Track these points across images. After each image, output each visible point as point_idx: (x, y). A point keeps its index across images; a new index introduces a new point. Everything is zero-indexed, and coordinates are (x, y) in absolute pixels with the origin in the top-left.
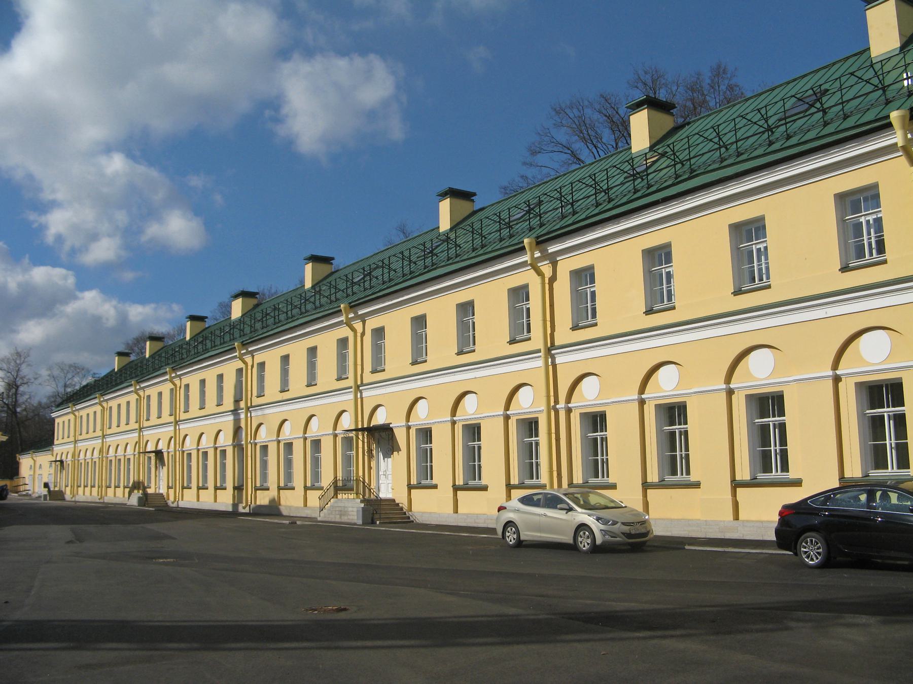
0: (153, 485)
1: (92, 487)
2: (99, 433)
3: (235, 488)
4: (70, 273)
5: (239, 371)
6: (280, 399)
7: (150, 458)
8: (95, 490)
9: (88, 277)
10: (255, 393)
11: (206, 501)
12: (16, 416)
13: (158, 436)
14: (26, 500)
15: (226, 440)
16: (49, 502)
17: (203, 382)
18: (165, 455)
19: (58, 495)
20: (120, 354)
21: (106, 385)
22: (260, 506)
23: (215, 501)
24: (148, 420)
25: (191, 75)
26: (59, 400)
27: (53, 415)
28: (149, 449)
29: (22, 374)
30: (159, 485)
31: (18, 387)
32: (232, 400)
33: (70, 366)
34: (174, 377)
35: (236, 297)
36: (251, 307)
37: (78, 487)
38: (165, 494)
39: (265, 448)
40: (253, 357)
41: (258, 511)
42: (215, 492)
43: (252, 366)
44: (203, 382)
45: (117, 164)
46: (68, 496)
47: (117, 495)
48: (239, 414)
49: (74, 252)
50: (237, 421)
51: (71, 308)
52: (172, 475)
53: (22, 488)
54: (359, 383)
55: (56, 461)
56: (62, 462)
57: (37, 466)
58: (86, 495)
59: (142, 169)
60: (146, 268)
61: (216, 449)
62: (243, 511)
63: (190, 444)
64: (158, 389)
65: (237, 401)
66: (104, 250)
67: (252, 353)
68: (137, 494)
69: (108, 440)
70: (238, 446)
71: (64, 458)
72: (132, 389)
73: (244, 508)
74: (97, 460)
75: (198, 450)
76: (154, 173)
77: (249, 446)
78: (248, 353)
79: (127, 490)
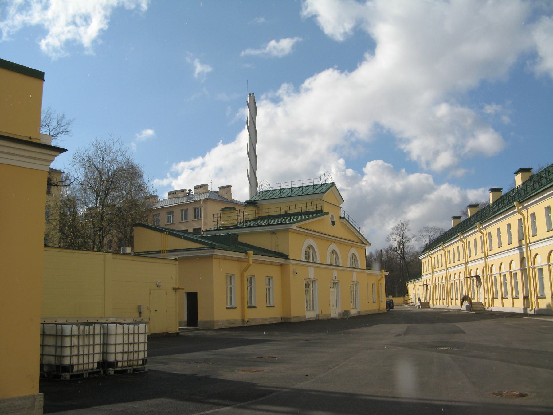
0: (476, 297)
2: (444, 267)
3: (524, 298)
4: (430, 175)
5: (520, 220)
7: (473, 281)
8: (445, 301)
9: (440, 177)
10: (531, 234)
11: (508, 306)
12: (405, 260)
13: (476, 267)
14: (411, 309)
15: (516, 266)
16: (421, 310)
17: (499, 230)
19: (426, 305)
20: (454, 218)
21: (446, 237)
22: (541, 309)
24: (470, 257)
25: (482, 49)
26: (422, 249)
28: (472, 275)
29: (405, 235)
31: (404, 243)
32: (517, 240)
33: (432, 229)
34: (482, 229)
35: (517, 173)
36: (528, 178)
37: (437, 300)
38: (483, 303)
39: (541, 270)
40: (527, 210)
41: (540, 313)
42: (513, 301)
43: (528, 217)
44: (499, 230)
45: (443, 110)
46: (431, 306)
47: (456, 305)
48: (522, 249)
49: (428, 163)
50: (521, 253)
51: (433, 196)
52: (486, 292)
53: (410, 301)
54: (528, 242)
55: (424, 285)
56: (427, 285)
57: (417, 288)
58: (440, 305)
59: (459, 109)
60: (472, 165)
61: (511, 272)
62: (531, 313)
63: (495, 271)
64: (474, 237)
65: (520, 241)
66: (444, 159)
67: (526, 208)
68: (466, 303)
69: (449, 271)
70: (523, 270)
71: (428, 283)
72: (459, 238)
73: (531, 311)
74: (445, 283)
76: (465, 110)
77: (531, 269)
78: (524, 208)
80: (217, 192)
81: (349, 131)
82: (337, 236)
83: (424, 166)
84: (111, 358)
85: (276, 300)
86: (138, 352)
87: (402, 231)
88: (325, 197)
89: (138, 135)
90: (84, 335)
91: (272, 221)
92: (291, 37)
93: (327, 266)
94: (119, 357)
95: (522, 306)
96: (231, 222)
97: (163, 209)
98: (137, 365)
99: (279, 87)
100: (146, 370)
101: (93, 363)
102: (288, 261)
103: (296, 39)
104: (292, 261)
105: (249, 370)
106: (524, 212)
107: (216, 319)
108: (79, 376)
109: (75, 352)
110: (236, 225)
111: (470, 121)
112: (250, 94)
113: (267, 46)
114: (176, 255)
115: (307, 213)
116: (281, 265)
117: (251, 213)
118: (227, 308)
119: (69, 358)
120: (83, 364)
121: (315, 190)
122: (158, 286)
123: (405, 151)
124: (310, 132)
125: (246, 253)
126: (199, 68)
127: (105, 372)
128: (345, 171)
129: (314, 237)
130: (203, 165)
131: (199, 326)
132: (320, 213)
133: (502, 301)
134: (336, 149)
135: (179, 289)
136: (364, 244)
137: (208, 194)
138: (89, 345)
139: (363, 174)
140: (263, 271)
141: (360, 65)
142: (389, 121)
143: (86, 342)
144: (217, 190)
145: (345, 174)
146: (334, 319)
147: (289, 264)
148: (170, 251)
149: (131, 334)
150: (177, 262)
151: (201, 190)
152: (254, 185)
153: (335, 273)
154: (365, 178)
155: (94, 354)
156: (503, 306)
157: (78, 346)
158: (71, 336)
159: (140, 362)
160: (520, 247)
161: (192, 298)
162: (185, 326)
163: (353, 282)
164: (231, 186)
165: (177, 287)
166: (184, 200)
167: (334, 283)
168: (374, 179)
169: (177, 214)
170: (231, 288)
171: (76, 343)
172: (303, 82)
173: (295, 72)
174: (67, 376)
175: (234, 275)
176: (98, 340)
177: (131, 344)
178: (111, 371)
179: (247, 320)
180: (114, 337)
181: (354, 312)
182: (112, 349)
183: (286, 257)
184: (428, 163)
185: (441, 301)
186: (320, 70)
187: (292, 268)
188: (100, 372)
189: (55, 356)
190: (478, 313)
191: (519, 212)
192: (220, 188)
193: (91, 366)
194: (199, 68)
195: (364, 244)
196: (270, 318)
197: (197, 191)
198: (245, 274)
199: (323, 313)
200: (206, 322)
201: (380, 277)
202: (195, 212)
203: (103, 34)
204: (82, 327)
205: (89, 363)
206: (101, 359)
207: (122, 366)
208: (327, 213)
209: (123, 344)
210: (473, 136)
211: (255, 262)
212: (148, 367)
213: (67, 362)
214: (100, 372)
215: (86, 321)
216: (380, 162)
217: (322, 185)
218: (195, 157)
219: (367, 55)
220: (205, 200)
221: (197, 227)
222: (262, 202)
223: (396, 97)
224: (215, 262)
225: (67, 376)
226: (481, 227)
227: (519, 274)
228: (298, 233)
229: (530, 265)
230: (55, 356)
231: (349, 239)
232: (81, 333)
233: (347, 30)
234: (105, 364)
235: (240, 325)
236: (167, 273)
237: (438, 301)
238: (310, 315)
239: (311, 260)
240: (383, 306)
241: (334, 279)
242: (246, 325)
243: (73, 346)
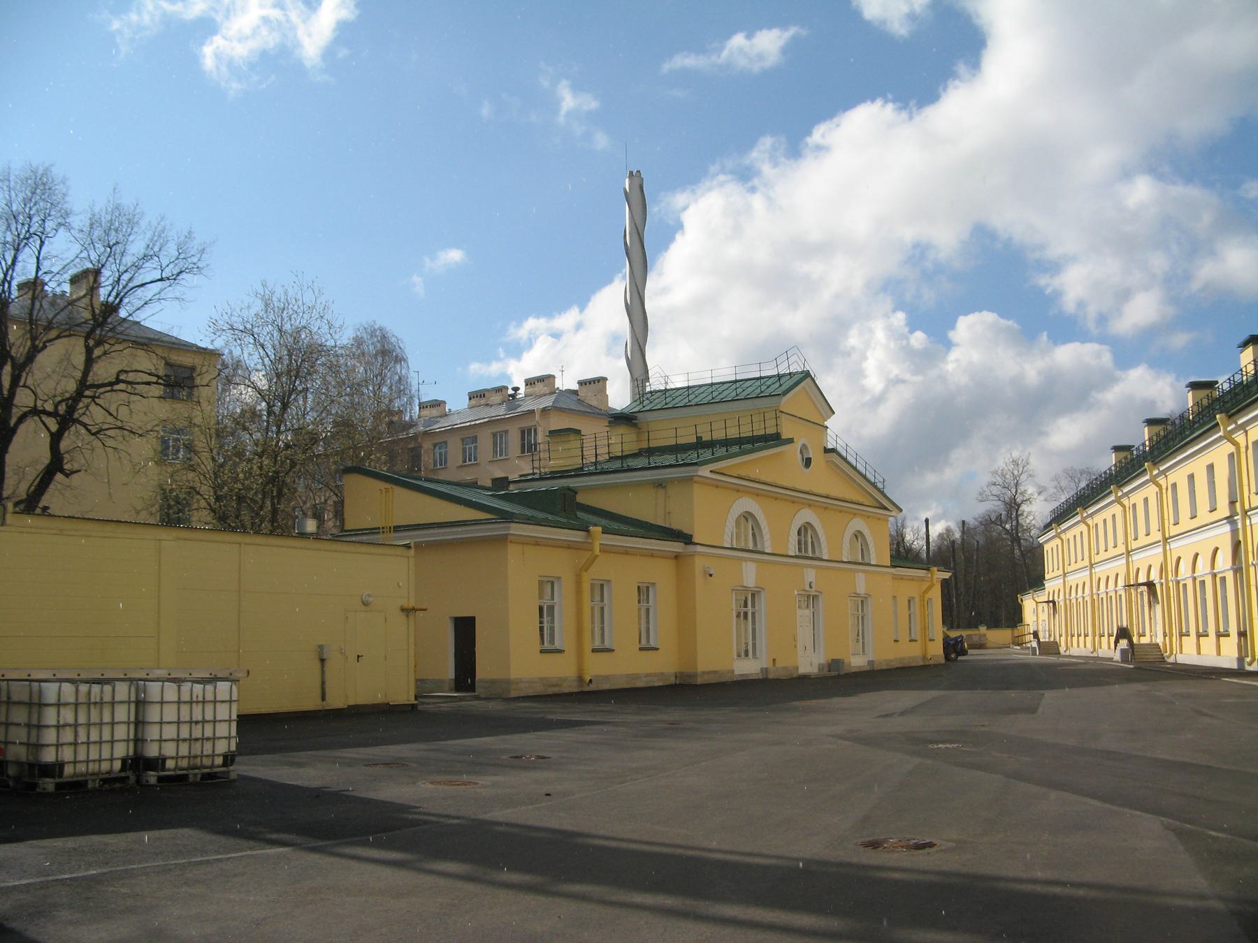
1: (1219, 635)
4: (1105, 347)
6: (840, 496)
7: (1142, 593)
8: (1089, 639)
9: (1129, 352)
13: (1148, 562)
15: (1224, 561)
16: (1039, 658)
18: (1158, 587)
19: (1050, 648)
23: (1219, 653)
27: (1041, 540)
30: (1152, 632)
31: (1019, 506)
32: (1227, 502)
35: (1245, 345)
37: (1102, 636)
43: (1247, 448)
45: (1142, 191)
47: (1109, 650)
49: (1102, 319)
50: (1234, 532)
51: (1111, 395)
54: (1247, 507)
55: (1048, 602)
56: (1054, 602)
59: (1179, 190)
65: (1232, 503)
66: (1143, 310)
70: (1238, 570)
72: (1112, 498)
75: (1194, 579)
76: (1194, 193)
78: (1239, 428)
79: (1113, 639)
80: (575, 392)
81: (916, 246)
82: (816, 491)
83: (1091, 326)
84: (152, 751)
85: (663, 630)
86: (214, 739)
87: (1015, 477)
88: (786, 403)
89: (427, 260)
90: (89, 704)
91: (657, 460)
92: (782, 24)
93: (766, 557)
94: (169, 750)
95: (1235, 654)
96: (568, 462)
97: (453, 431)
98: (212, 766)
99: (751, 144)
100: (233, 776)
101: (112, 760)
102: (691, 548)
103: (792, 31)
104: (699, 549)
105: (450, 783)
106: (1240, 437)
107: (514, 675)
108: (77, 785)
109: (68, 736)
110: (582, 469)
111: (1207, 218)
112: (631, 173)
113: (723, 48)
114: (410, 537)
115: (740, 441)
116: (677, 557)
117: (622, 441)
118: (541, 652)
119: (53, 749)
120: (88, 762)
121: (763, 388)
122: (365, 604)
123: (1048, 292)
124: (824, 249)
125: (588, 531)
126: (568, 101)
127: (138, 781)
128: (908, 339)
129: (757, 494)
130: (579, 327)
131: (479, 691)
132: (774, 439)
133: (1198, 640)
134: (890, 289)
135: (414, 610)
136: (886, 509)
137: (553, 397)
138: (101, 724)
139: (949, 345)
140: (625, 569)
141: (945, 89)
142: (1014, 220)
143: (95, 718)
144: (575, 387)
145: (908, 344)
146: (804, 678)
147: (693, 555)
148: (397, 529)
149: (197, 702)
150: (412, 552)
151: (540, 388)
152: (638, 374)
153: (810, 575)
154: (954, 355)
155: (112, 742)
156: (1199, 653)
157: (76, 726)
158: (59, 705)
159: (219, 761)
160: (1230, 519)
161: (465, 629)
162: (451, 691)
163: (858, 595)
164: (605, 379)
165: (412, 604)
166: (501, 411)
167: (808, 596)
168: (976, 356)
169: (485, 442)
170: (602, 609)
171: (71, 720)
172: (809, 133)
173: (790, 111)
174: (49, 784)
175: (559, 578)
176: (122, 713)
177: (197, 722)
178: (152, 777)
179: (588, 678)
180: (158, 707)
181: (857, 662)
182: (152, 733)
183: (687, 539)
184: (1102, 319)
185: (1082, 638)
186: (849, 103)
187: (699, 564)
188: (128, 778)
189: (28, 744)
190: (1146, 667)
191: (1228, 437)
192: (581, 383)
193: (105, 766)
194: (568, 101)
195: (886, 509)
196: (647, 675)
197: (530, 390)
198: (586, 578)
199: (778, 665)
200: (493, 682)
201: (926, 585)
202: (523, 439)
203: (344, 31)
204: (84, 688)
205: (100, 761)
206: (131, 753)
207: (176, 768)
208: (791, 441)
209: (179, 723)
210: (1212, 253)
211: (606, 549)
212: (237, 770)
213: (49, 756)
214: (128, 778)
215: (98, 676)
216: (989, 317)
217: (779, 377)
218: (563, 308)
219: (962, 68)
220: (544, 410)
221: (499, 474)
222: (650, 416)
223: (1031, 160)
224: (513, 551)
225: (49, 784)
226: (1155, 472)
227: (1230, 577)
228: (717, 485)
229: (1251, 560)
230: (28, 744)
231: (848, 497)
232: (82, 699)
233: (918, 9)
234: (138, 763)
235: (573, 688)
236: (386, 575)
237: (1075, 639)
238: (748, 668)
239: (751, 547)
240: (936, 650)
241: (807, 588)
242: (587, 689)
243: (64, 726)
